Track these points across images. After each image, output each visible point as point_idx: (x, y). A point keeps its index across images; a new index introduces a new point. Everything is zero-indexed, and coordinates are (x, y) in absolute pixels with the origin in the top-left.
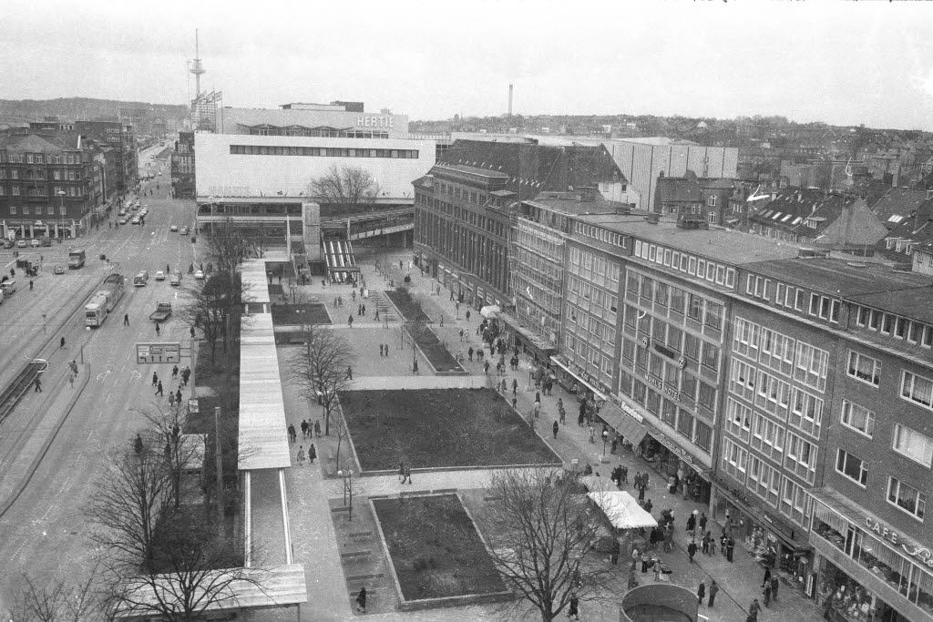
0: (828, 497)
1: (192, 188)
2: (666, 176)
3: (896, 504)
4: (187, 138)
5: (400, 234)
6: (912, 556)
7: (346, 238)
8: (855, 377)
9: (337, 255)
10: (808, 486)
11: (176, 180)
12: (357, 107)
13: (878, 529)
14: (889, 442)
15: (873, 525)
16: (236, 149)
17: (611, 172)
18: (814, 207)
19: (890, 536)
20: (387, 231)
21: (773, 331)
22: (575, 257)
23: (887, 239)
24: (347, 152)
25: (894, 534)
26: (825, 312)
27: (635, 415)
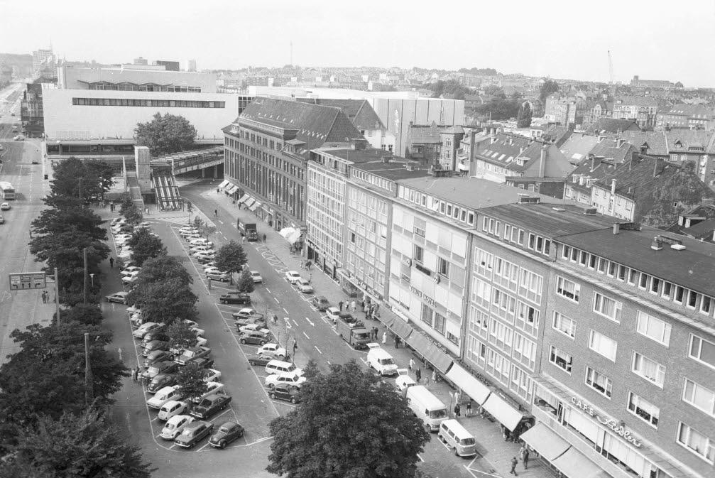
0: (544, 381)
1: (41, 129)
2: (413, 124)
3: (634, 413)
4: (34, 89)
5: (212, 168)
6: (605, 425)
7: (171, 174)
8: (562, 295)
9: (164, 187)
10: (530, 372)
11: (26, 122)
12: (173, 66)
13: (580, 405)
14: (587, 342)
15: (576, 402)
16: (76, 101)
17: (374, 121)
18: (521, 149)
19: (588, 410)
20: (203, 166)
21: (511, 263)
22: (353, 193)
23: (574, 175)
24: (168, 103)
25: (591, 409)
26: (540, 246)
27: (402, 316)
